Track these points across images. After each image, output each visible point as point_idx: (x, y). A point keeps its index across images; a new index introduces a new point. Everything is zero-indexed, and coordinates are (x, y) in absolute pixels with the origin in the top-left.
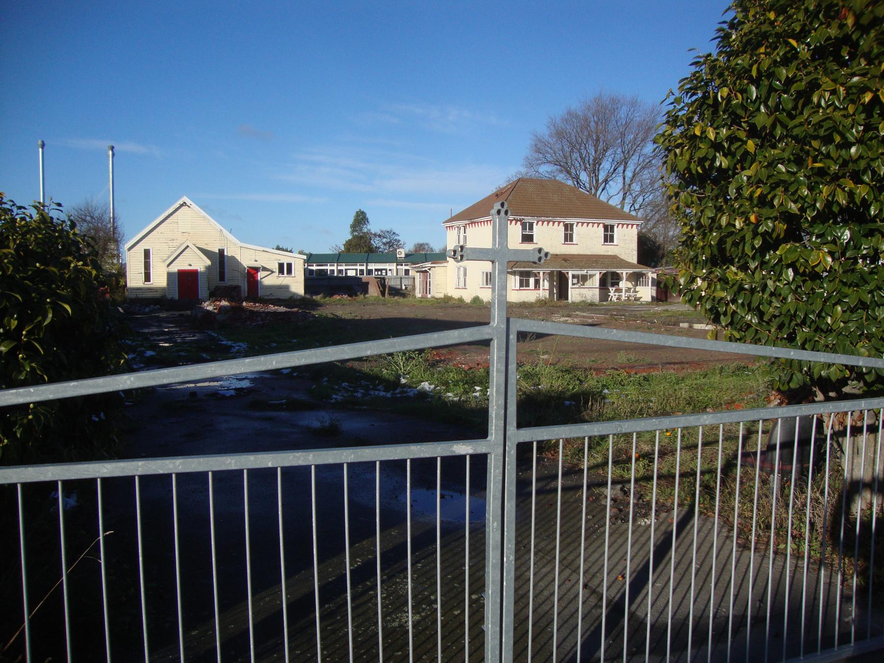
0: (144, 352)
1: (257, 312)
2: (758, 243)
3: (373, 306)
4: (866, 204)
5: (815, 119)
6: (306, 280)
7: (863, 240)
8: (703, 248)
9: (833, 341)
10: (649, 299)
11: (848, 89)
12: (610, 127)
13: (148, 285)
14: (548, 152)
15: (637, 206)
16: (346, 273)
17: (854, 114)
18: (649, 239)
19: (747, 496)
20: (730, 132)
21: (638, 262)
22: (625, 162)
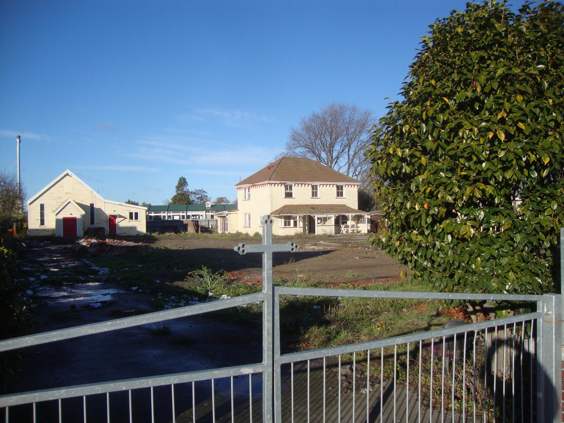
0: (39, 276)
1: (115, 246)
2: (429, 220)
3: (190, 241)
4: (492, 197)
5: (462, 147)
6: (147, 223)
7: (492, 216)
8: (396, 220)
9: (476, 279)
10: (366, 232)
11: (479, 129)
12: (340, 124)
13: (43, 227)
14: (301, 140)
15: (357, 173)
16: (173, 218)
17: (483, 144)
18: (365, 194)
19: (426, 371)
20: (411, 153)
21: (359, 209)
22: (349, 146)
